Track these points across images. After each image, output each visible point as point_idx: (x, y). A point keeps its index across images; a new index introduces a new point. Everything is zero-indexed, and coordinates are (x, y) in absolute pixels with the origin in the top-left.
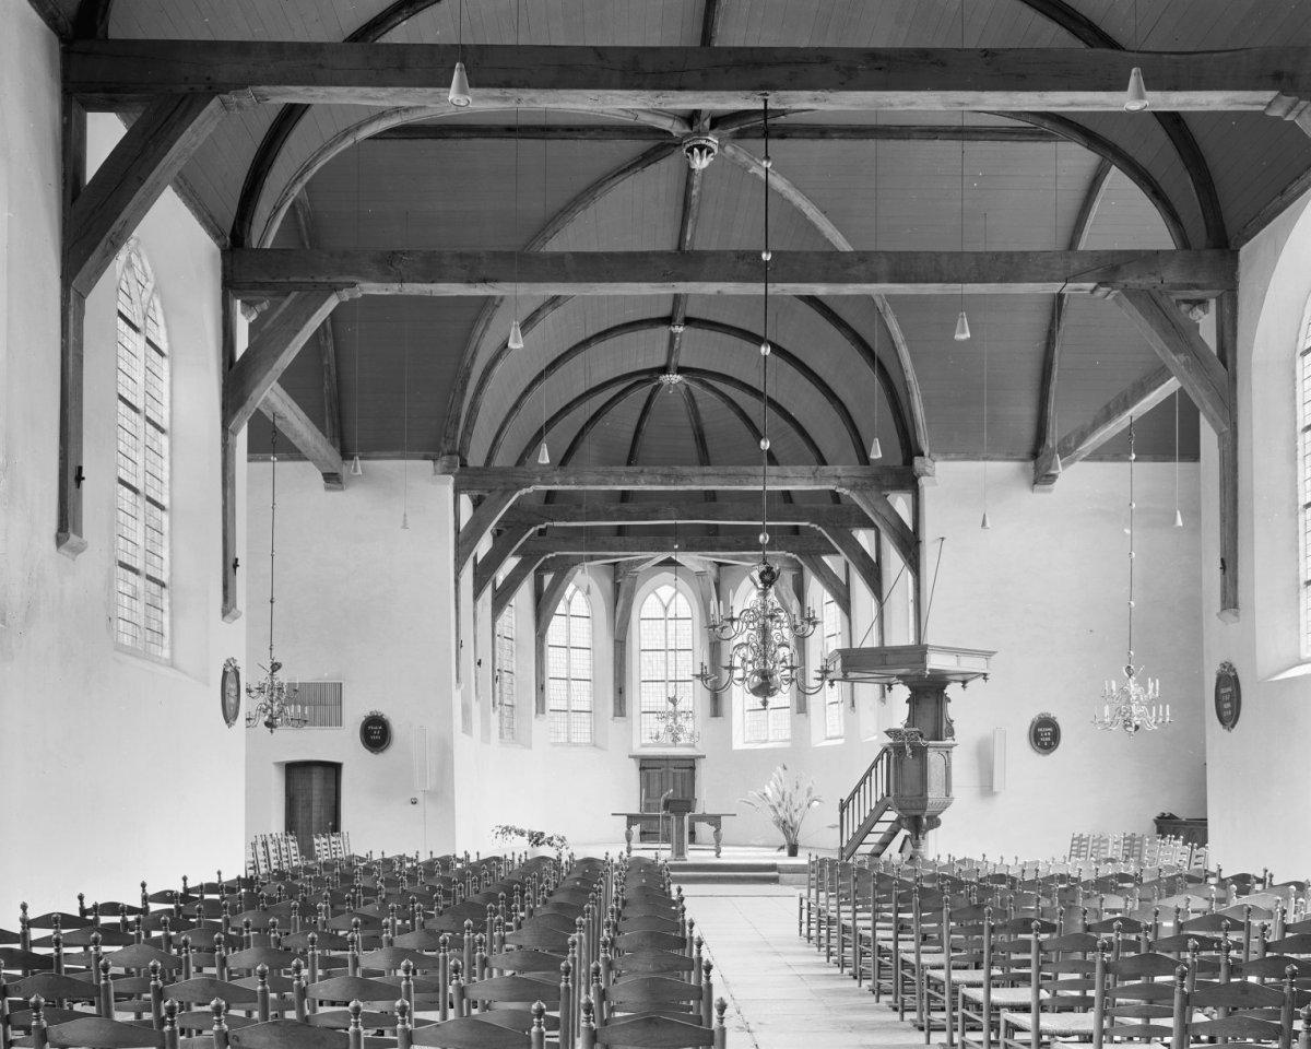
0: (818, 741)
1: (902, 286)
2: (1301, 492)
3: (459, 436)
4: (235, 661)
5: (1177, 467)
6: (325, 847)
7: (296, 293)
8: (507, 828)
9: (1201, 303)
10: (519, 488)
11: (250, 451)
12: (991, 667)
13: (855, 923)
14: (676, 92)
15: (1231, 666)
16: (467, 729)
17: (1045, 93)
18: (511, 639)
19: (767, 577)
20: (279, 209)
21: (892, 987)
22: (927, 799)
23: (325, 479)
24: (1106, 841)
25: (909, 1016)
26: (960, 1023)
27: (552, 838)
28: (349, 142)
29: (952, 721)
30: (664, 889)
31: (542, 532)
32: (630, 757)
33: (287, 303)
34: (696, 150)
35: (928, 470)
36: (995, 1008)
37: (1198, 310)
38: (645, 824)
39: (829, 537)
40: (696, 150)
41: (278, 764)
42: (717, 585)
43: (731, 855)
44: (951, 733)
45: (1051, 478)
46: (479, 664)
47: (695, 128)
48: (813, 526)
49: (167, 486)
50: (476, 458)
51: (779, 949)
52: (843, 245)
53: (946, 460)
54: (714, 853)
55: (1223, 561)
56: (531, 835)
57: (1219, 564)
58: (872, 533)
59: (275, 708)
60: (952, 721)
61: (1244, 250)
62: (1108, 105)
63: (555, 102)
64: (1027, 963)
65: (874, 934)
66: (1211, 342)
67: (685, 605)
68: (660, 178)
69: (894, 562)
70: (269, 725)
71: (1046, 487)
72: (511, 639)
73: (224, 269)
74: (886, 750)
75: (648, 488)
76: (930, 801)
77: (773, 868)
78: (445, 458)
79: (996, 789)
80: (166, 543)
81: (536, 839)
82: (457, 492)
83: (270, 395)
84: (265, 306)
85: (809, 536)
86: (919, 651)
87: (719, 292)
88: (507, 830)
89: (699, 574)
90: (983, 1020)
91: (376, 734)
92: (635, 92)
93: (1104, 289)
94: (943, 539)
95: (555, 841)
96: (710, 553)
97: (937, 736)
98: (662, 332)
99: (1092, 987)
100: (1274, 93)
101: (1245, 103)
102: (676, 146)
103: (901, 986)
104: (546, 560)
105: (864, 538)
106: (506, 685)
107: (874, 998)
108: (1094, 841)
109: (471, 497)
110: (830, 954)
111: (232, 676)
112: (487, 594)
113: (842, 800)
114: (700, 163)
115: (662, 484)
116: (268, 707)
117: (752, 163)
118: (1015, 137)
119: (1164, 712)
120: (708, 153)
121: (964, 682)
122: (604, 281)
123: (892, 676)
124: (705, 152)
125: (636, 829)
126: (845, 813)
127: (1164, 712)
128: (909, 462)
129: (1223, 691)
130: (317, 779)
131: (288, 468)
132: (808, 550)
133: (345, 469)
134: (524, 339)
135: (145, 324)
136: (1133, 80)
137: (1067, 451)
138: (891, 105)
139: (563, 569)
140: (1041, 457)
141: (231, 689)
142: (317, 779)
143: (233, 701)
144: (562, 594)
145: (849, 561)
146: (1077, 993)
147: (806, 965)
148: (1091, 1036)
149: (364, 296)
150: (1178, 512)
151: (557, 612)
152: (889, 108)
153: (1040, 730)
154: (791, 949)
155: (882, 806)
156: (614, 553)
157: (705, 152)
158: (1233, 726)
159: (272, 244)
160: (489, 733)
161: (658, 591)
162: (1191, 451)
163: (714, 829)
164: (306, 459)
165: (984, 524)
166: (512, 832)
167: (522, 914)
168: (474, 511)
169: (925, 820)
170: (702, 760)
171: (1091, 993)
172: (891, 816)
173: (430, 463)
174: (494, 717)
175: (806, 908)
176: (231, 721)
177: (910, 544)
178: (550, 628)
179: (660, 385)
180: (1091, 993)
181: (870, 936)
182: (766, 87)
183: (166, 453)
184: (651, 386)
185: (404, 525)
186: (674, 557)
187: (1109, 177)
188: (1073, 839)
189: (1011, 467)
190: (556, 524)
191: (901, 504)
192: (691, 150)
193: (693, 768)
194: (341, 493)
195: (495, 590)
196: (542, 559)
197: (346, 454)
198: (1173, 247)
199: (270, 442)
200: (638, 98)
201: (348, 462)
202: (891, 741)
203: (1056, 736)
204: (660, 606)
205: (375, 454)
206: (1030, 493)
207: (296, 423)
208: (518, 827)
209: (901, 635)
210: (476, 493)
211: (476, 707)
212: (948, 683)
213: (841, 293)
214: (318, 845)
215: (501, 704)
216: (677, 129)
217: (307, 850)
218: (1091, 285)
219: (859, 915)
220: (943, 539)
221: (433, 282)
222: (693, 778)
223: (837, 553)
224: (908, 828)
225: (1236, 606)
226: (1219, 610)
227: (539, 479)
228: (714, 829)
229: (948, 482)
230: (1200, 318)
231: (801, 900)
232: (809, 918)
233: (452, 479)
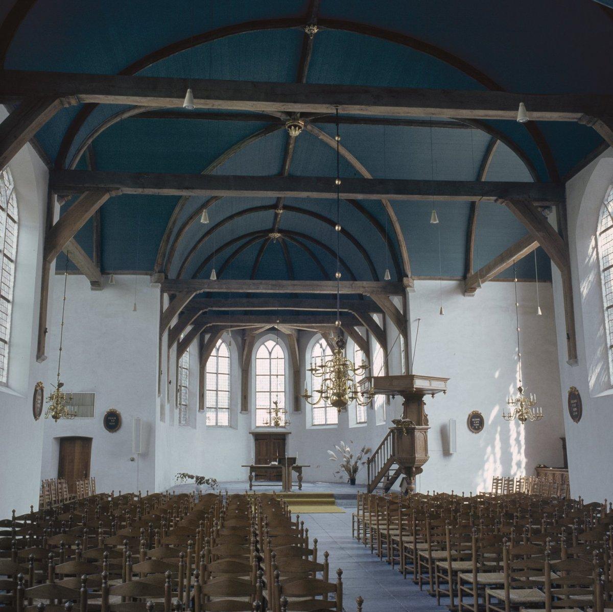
0: (352, 424)
1: (400, 196)
2: (605, 300)
3: (164, 264)
4: (41, 383)
5: (537, 285)
6: (82, 486)
7: (87, 192)
8: (183, 474)
9: (548, 207)
10: (196, 290)
11: (56, 269)
12: (447, 386)
13: (388, 531)
14: (293, 104)
15: (576, 388)
16: (162, 418)
17: (473, 111)
18: (187, 369)
19: (340, 344)
20: (81, 149)
21: (414, 570)
22: (415, 458)
23: (91, 284)
24: (513, 480)
25: (425, 587)
26: (436, 580)
27: (209, 480)
28: (118, 119)
29: (427, 415)
30: (285, 514)
31: (204, 313)
32: (250, 433)
33: (82, 197)
34: (293, 127)
35: (410, 284)
36: (455, 573)
37: (547, 211)
38: (258, 472)
39: (359, 318)
40: (293, 127)
41: (56, 439)
42: (298, 341)
43: (307, 488)
44: (426, 422)
45: (473, 289)
46: (170, 383)
47: (292, 117)
48: (350, 311)
49: (12, 289)
50: (172, 275)
51: (343, 546)
52: (367, 175)
53: (420, 279)
54: (298, 487)
55: (567, 334)
56: (197, 478)
57: (566, 336)
58: (381, 315)
59: (59, 408)
60: (427, 415)
61: (568, 184)
62: (504, 117)
63: (231, 106)
64: (470, 548)
65: (401, 539)
66: (555, 226)
67: (279, 352)
68: (273, 139)
69: (393, 331)
70: (54, 417)
71: (471, 294)
72: (187, 369)
73: (50, 180)
74: (392, 431)
75: (264, 291)
76: (417, 459)
77: (331, 496)
78: (156, 274)
79: (451, 452)
80: (9, 320)
81: (200, 480)
82: (162, 292)
83: (68, 244)
84: (70, 198)
85: (353, 318)
86: (410, 378)
87: (308, 196)
88: (184, 475)
89: (289, 335)
90: (449, 578)
91: (113, 421)
92: (272, 103)
93: (501, 200)
94: (419, 319)
95: (210, 481)
96: (295, 325)
97: (419, 424)
98: (272, 211)
99: (502, 560)
100: (582, 114)
101: (569, 118)
102: (283, 125)
103: (420, 571)
104: (207, 327)
105: (376, 318)
106: (183, 394)
107: (403, 577)
108: (505, 481)
109: (168, 294)
110: (373, 549)
111: (40, 391)
112: (175, 346)
113: (369, 458)
114: (295, 133)
115: (271, 289)
116: (55, 408)
117: (320, 133)
118: (450, 126)
119: (539, 410)
120: (299, 129)
121: (433, 394)
122: (249, 190)
123: (395, 391)
124: (297, 128)
125: (253, 474)
126: (370, 465)
127: (539, 410)
128: (401, 280)
129: (572, 402)
130: (78, 448)
131: (72, 278)
132: (349, 324)
133: (102, 279)
134: (203, 215)
135: (7, 206)
136: (520, 108)
137: (483, 275)
138: (399, 113)
139: (215, 333)
140: (467, 280)
141: (39, 399)
142: (78, 448)
143: (39, 406)
144: (214, 346)
145: (369, 329)
146: (495, 563)
147: (352, 549)
148: (544, 603)
149: (123, 194)
150: (539, 308)
151: (212, 354)
152: (398, 115)
153: (473, 420)
154: (350, 545)
155: (390, 462)
156: (244, 324)
157: (297, 128)
158: (579, 420)
159: (76, 167)
160: (173, 421)
161: (265, 343)
162: (546, 277)
163: (298, 474)
164: (82, 274)
165: (441, 313)
166: (187, 477)
167: (178, 519)
168: (170, 304)
169: (414, 469)
170: (290, 435)
171: (501, 564)
172: (395, 466)
173: (148, 277)
174: (177, 411)
175: (359, 523)
176: (37, 417)
177: (403, 323)
178: (208, 362)
179: (269, 238)
180: (501, 564)
181: (386, 533)
182: (337, 103)
183: (12, 272)
184: (263, 239)
185: (132, 309)
186: (276, 327)
187: (496, 146)
188: (494, 480)
189: (452, 283)
190: (214, 309)
191: (397, 301)
192: (290, 127)
193: (284, 440)
194: (100, 292)
195: (179, 343)
196: (205, 327)
197: (103, 271)
198: (532, 180)
199: (66, 266)
200: (274, 106)
201: (105, 276)
202: (395, 426)
203: (482, 423)
204: (268, 352)
205: (119, 271)
206: (463, 297)
207: (78, 256)
208: (190, 474)
209: (398, 370)
210: (172, 293)
211: (167, 407)
212: (424, 395)
213: (370, 199)
214: (79, 489)
215: (180, 404)
216: (283, 117)
217: (72, 489)
218: (495, 198)
219: (380, 522)
220: (419, 319)
221: (160, 188)
222: (284, 445)
223: (362, 325)
224: (405, 474)
225: (576, 357)
226: (567, 360)
227: (206, 286)
228: (298, 474)
229: (422, 291)
230: (548, 215)
231: (353, 516)
232: (359, 527)
233: (160, 285)
